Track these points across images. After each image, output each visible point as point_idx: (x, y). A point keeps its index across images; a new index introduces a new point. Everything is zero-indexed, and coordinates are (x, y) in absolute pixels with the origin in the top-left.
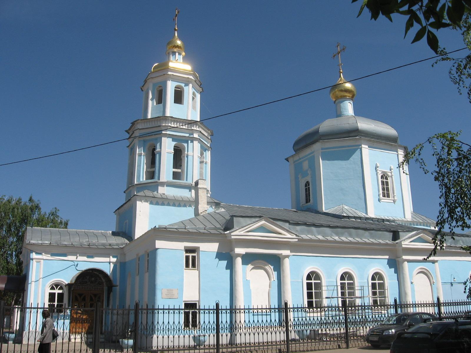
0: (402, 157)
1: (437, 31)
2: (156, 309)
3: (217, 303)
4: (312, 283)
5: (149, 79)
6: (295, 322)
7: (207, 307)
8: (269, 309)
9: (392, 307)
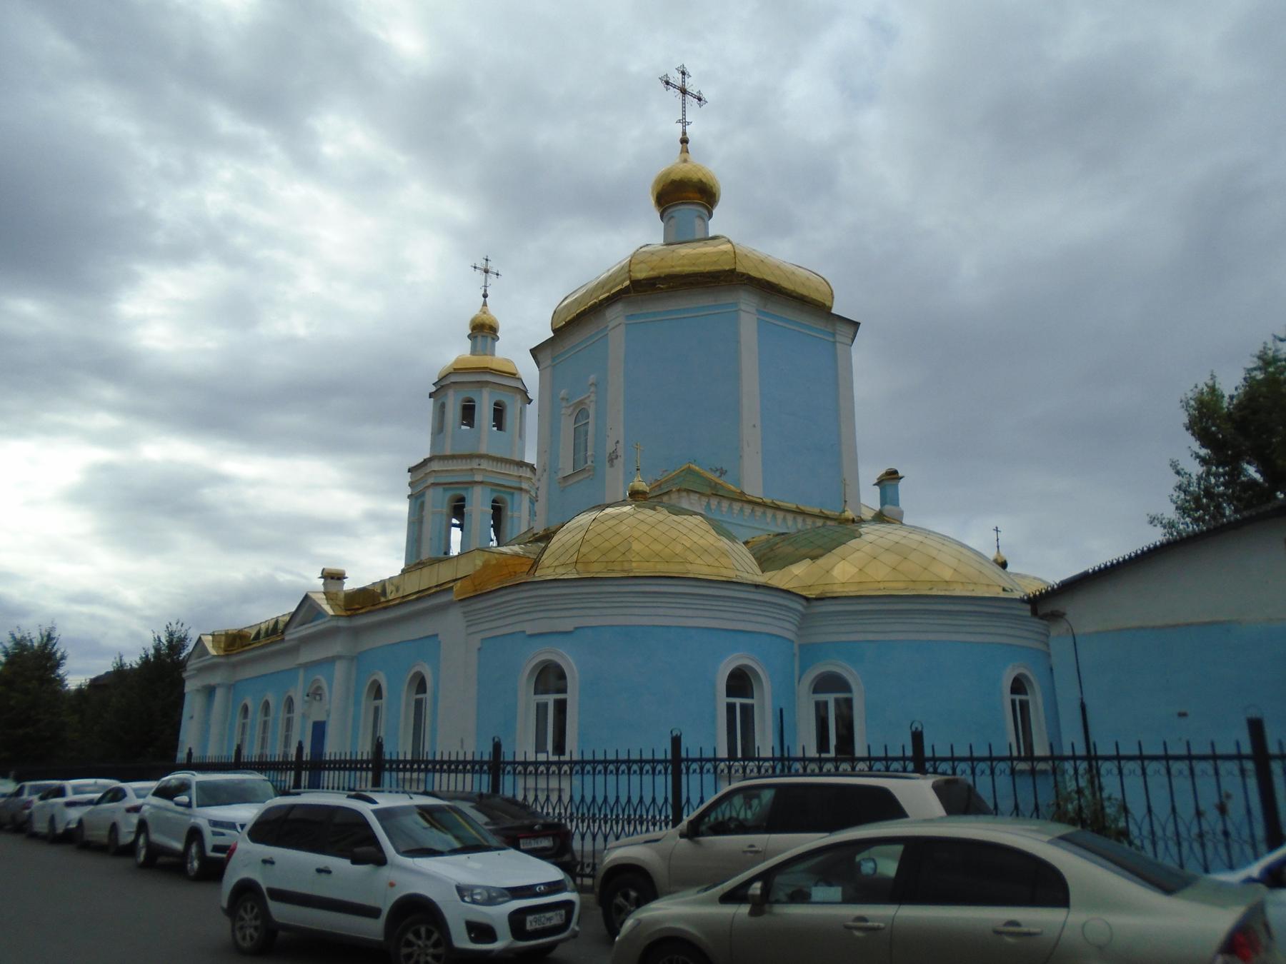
1: (497, 747)
2: (1067, 758)
3: (916, 728)
9: (660, 767)
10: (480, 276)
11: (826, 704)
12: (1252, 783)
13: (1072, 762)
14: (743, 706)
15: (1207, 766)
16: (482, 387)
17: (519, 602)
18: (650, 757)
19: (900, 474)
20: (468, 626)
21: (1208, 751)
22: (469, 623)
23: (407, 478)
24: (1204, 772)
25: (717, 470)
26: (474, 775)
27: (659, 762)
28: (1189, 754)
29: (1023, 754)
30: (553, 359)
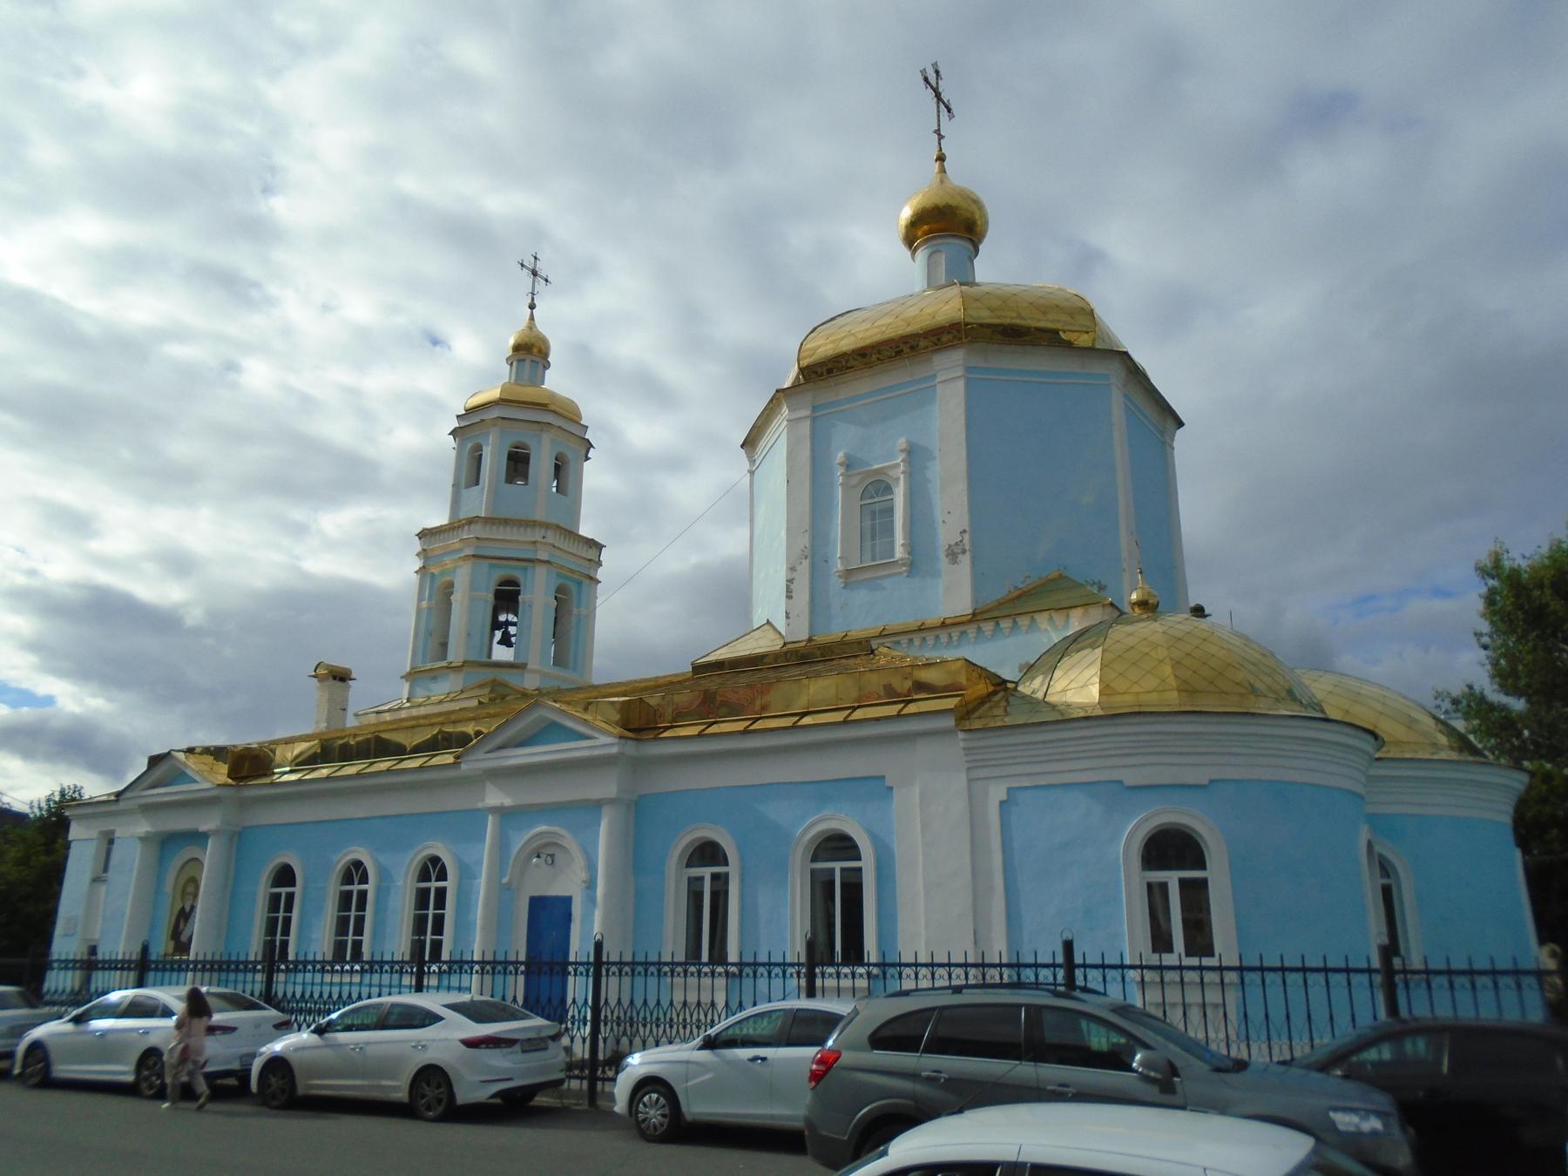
4: (833, 870)
5: (938, 112)
7: (777, 958)
8: (1009, 966)
10: (526, 276)
11: (1164, 887)
12: (1380, 998)
13: (1082, 970)
14: (715, 877)
15: (1320, 977)
16: (542, 430)
17: (1112, 739)
18: (643, 960)
19: (1207, 612)
20: (969, 769)
21: (1342, 965)
22: (974, 764)
23: (417, 546)
24: (1114, 979)
25: (1094, 583)
27: (626, 964)
28: (1221, 965)
30: (814, 409)
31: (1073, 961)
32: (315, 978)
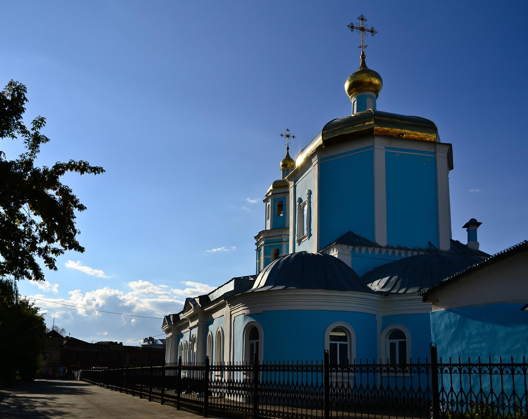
0: (139, 283)
6: (463, 397)
26: (216, 372)
29: (389, 363)
31: (489, 364)
32: (301, 411)
